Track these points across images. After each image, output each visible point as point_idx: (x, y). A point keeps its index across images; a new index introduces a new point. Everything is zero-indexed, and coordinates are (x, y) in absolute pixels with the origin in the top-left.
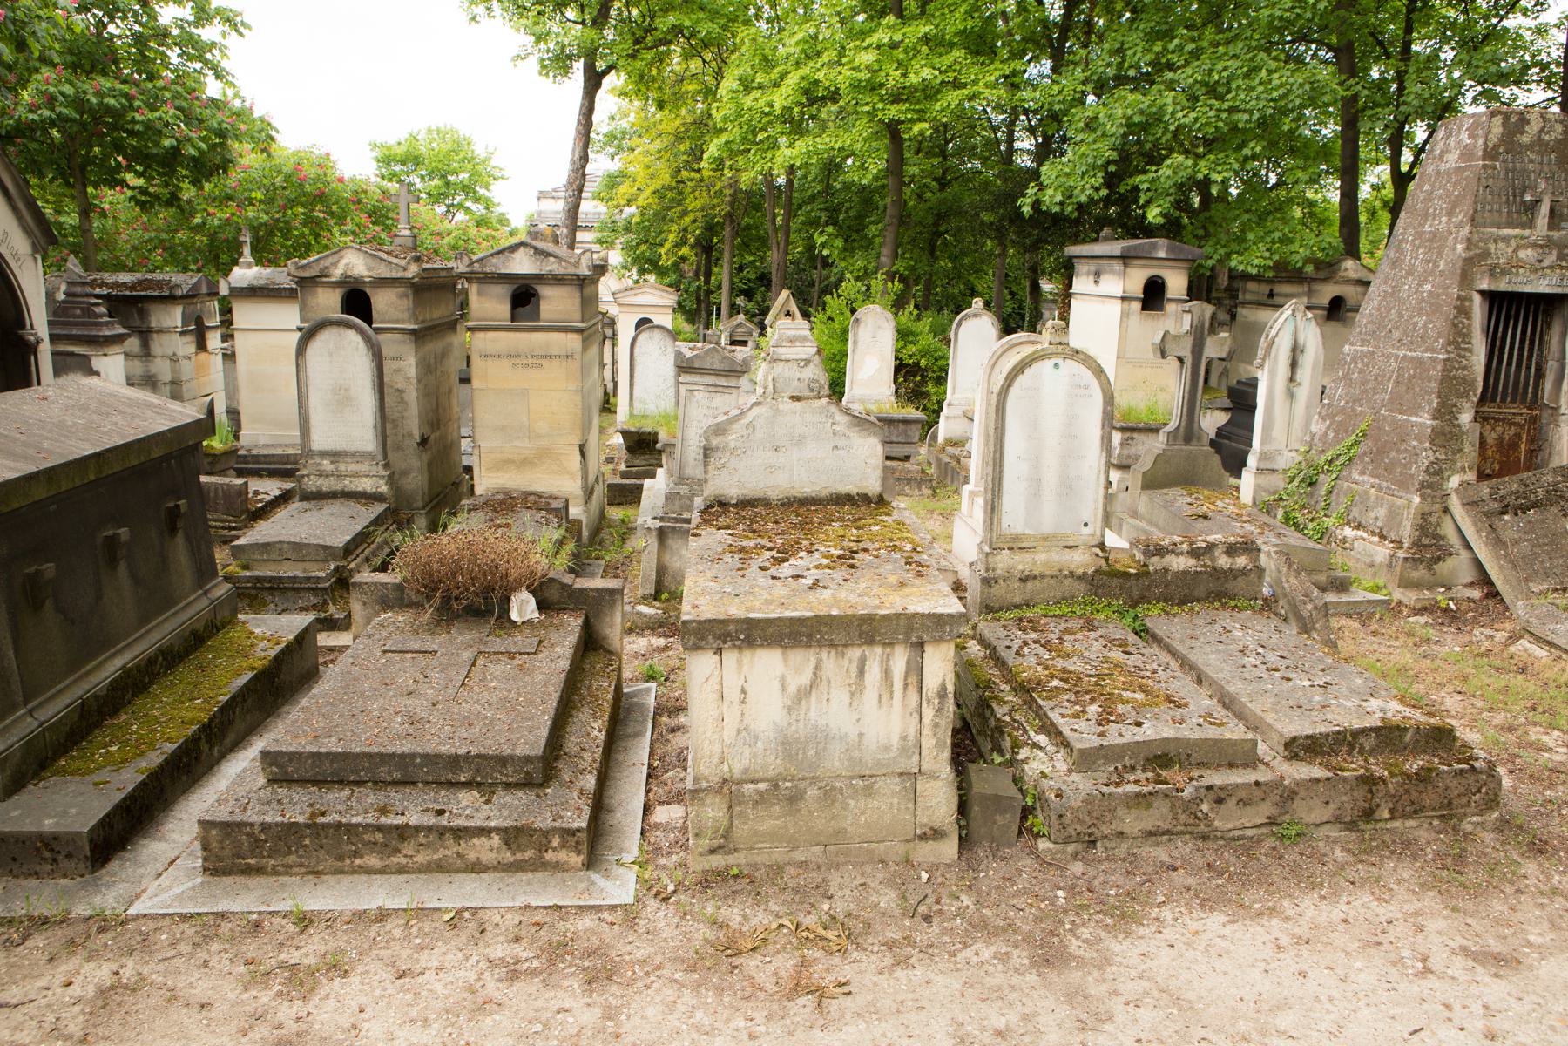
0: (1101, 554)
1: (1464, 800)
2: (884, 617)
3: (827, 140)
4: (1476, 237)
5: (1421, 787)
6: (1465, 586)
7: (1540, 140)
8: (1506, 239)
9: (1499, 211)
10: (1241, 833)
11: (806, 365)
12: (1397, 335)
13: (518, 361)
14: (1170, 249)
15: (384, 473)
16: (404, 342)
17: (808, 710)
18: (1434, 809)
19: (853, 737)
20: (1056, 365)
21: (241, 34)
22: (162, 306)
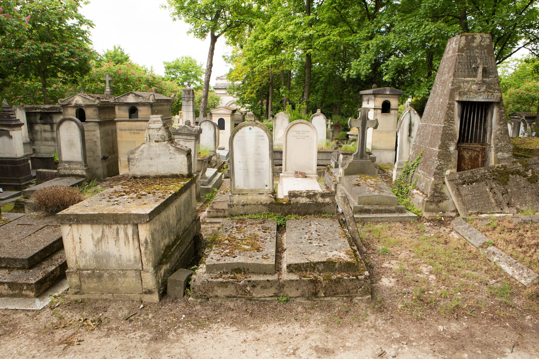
0: (272, 196)
1: (355, 291)
2: (121, 214)
3: (280, 56)
4: (455, 81)
5: (336, 285)
6: (451, 212)
7: (480, 44)
8: (467, 82)
9: (464, 71)
10: (264, 299)
11: (159, 130)
12: (432, 118)
13: (132, 132)
14: (391, 91)
15: (85, 168)
16: (96, 126)
17: (102, 246)
18: (342, 294)
19: (118, 256)
20: (250, 128)
21: (93, 28)
22: (57, 115)
